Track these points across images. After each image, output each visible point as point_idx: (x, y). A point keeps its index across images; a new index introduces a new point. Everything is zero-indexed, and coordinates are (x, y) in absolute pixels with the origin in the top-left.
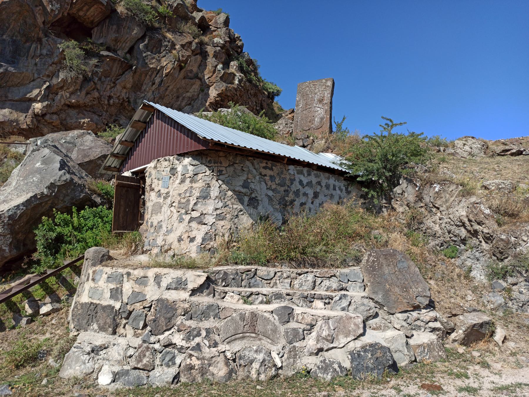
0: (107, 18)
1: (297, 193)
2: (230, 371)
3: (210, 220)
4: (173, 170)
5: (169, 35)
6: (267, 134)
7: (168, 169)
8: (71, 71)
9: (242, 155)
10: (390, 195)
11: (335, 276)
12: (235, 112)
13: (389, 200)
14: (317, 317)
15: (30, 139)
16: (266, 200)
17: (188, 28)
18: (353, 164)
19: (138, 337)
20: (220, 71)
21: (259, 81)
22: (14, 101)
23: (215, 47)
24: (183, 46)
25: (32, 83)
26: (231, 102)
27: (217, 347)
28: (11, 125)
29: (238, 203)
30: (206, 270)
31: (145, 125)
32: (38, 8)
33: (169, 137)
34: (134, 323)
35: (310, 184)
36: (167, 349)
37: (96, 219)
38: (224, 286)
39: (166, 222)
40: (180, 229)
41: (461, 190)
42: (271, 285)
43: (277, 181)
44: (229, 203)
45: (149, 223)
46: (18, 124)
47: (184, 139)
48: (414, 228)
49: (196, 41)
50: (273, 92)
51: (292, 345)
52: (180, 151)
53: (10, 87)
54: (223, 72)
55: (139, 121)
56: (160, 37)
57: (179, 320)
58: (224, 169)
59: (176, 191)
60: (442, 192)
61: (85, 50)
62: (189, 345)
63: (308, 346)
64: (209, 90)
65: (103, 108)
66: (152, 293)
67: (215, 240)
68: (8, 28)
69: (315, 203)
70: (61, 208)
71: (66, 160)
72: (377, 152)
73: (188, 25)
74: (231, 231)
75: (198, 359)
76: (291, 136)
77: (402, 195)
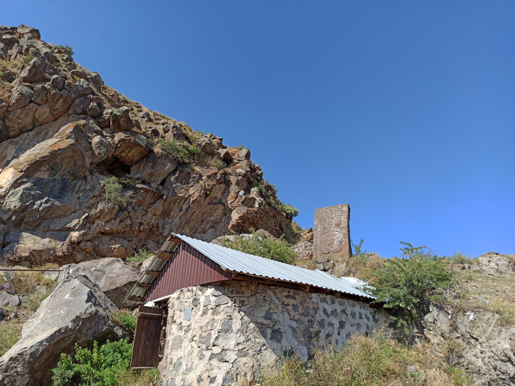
0: (144, 157)
1: (322, 323)
3: (232, 356)
4: (196, 301)
5: (197, 169)
6: (287, 257)
7: (191, 300)
8: (109, 202)
9: (264, 284)
10: (420, 323)
12: (256, 237)
13: (421, 329)
15: (64, 266)
16: (290, 332)
17: (214, 162)
18: (377, 290)
21: (277, 204)
22: (54, 231)
23: (237, 176)
24: (209, 177)
25: (73, 214)
26: (252, 228)
28: (49, 253)
29: (261, 336)
31: (171, 255)
32: (88, 153)
33: (193, 267)
35: (334, 313)
37: (116, 354)
39: (186, 359)
40: (200, 367)
41: (498, 319)
43: (301, 310)
44: (251, 336)
45: (169, 360)
46: (55, 252)
47: (208, 270)
48: (454, 363)
49: (221, 172)
50: (291, 213)
52: (203, 281)
53: (53, 218)
54: (244, 197)
55: (166, 251)
56: (189, 170)
58: (246, 299)
59: (197, 324)
60: (477, 320)
61: (122, 184)
64: (231, 214)
65: (134, 233)
67: (236, 380)
68: (60, 170)
69: (341, 333)
70: (83, 343)
71: (94, 290)
72: (402, 277)
73: (214, 159)
74: (254, 370)
76: (311, 259)
77: (434, 323)
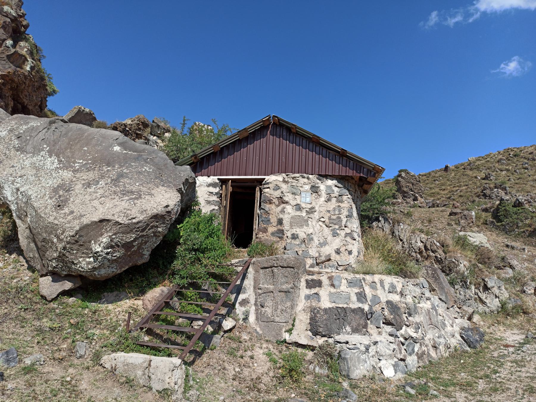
20: (8, 47)
66: (384, 297)
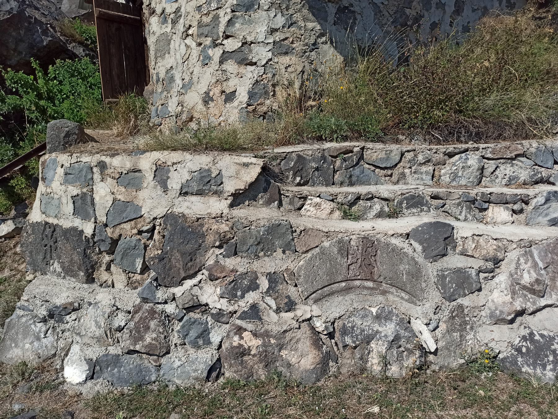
2: (324, 357)
3: (262, 54)
11: (523, 155)
14: (505, 242)
16: (369, 12)
19: (135, 288)
27: (295, 310)
30: (261, 153)
34: (125, 261)
36: (191, 314)
38: (299, 184)
39: (180, 69)
40: (205, 78)
42: (395, 178)
44: (297, 17)
51: (454, 303)
57: (211, 257)
62: (236, 307)
63: (490, 304)
66: (152, 203)
67: (274, 95)
75: (255, 335)
